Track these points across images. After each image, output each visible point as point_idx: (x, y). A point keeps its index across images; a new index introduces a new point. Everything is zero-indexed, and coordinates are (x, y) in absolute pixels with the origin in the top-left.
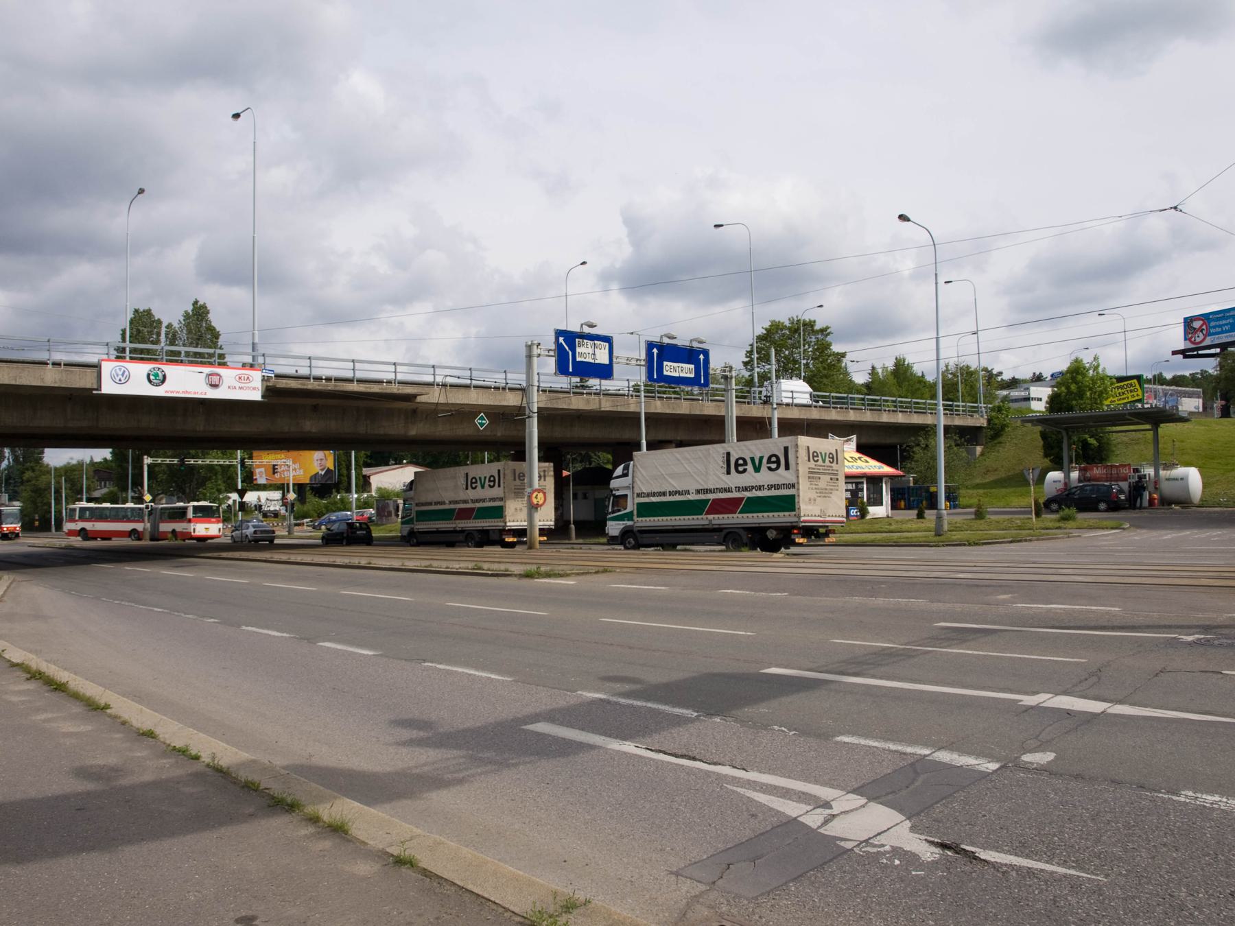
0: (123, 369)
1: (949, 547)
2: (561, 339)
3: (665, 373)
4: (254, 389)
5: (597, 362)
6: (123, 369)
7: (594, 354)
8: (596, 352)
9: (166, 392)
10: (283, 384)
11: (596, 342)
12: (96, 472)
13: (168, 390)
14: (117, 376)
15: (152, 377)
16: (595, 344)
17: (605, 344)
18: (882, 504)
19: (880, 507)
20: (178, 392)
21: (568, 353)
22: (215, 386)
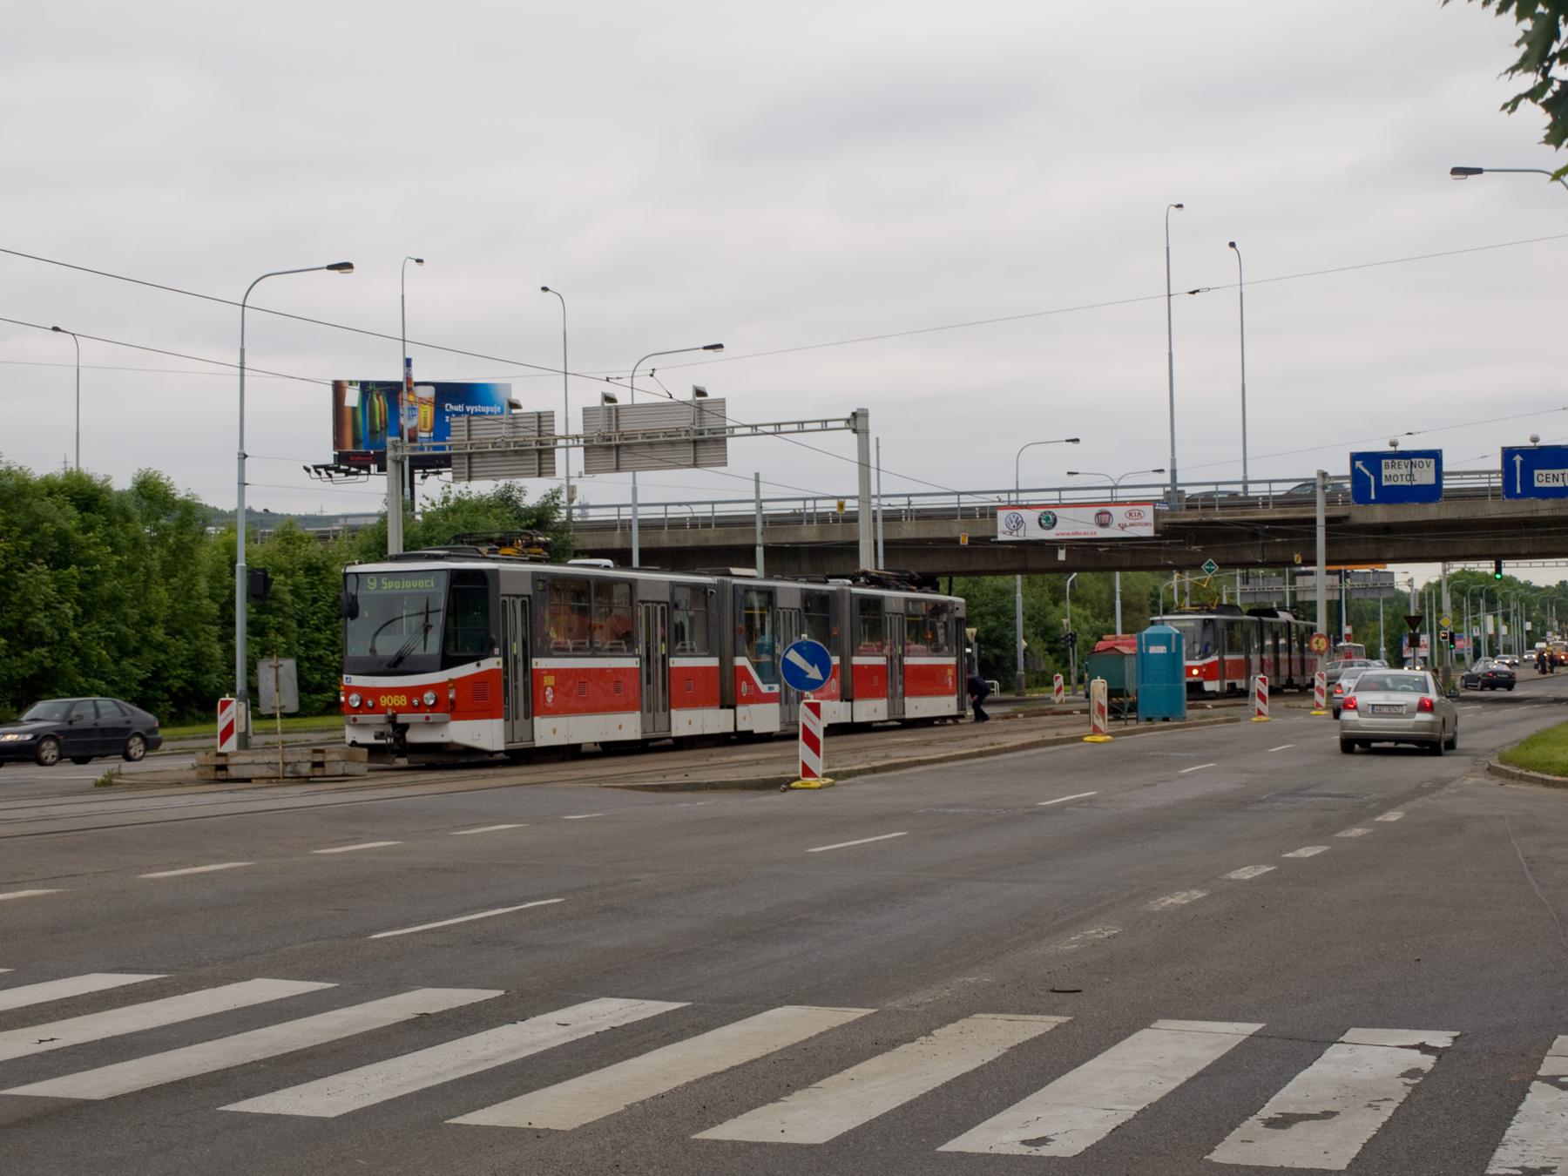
0: (1016, 516)
1: (646, 793)
2: (1359, 464)
3: (1537, 484)
4: (1146, 524)
5: (1414, 483)
6: (1016, 516)
7: (1410, 476)
8: (1413, 472)
9: (1057, 534)
10: (909, 531)
11: (1413, 460)
12: (972, 623)
13: (1057, 532)
14: (1012, 522)
15: (1043, 522)
16: (1412, 462)
17: (1428, 460)
18: (819, 704)
19: (821, 706)
20: (1068, 534)
21: (1370, 478)
22: (1104, 525)
